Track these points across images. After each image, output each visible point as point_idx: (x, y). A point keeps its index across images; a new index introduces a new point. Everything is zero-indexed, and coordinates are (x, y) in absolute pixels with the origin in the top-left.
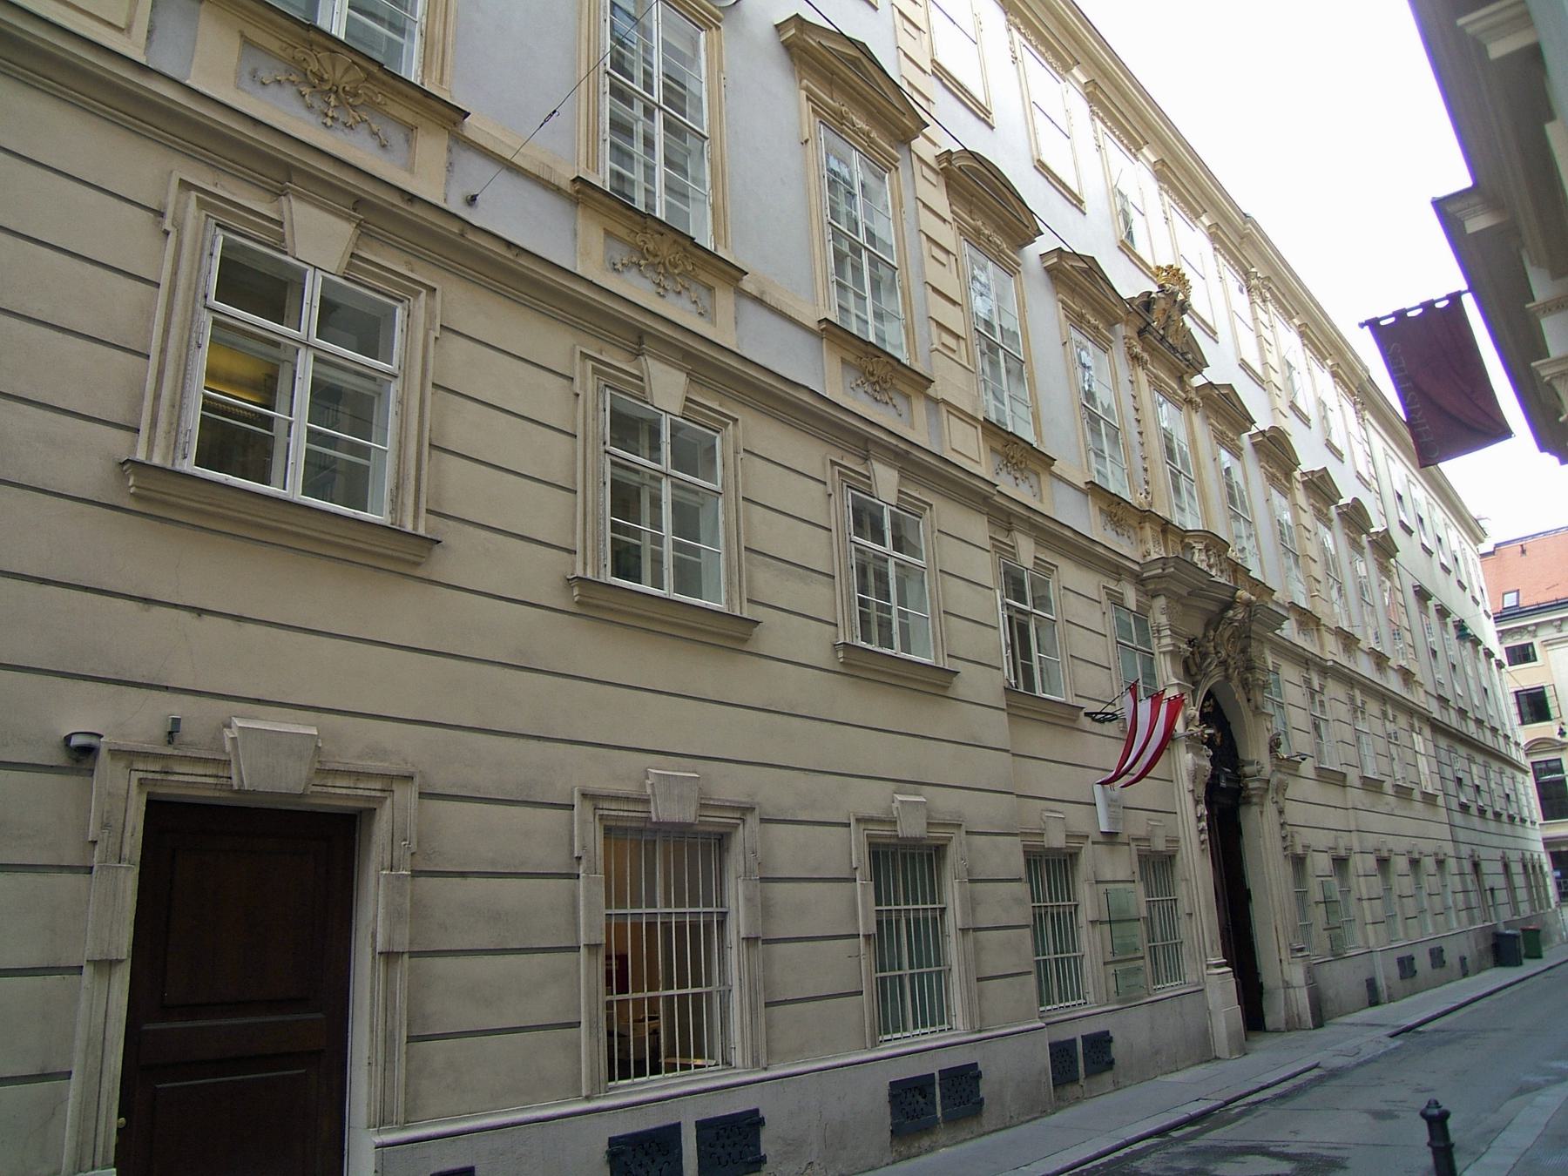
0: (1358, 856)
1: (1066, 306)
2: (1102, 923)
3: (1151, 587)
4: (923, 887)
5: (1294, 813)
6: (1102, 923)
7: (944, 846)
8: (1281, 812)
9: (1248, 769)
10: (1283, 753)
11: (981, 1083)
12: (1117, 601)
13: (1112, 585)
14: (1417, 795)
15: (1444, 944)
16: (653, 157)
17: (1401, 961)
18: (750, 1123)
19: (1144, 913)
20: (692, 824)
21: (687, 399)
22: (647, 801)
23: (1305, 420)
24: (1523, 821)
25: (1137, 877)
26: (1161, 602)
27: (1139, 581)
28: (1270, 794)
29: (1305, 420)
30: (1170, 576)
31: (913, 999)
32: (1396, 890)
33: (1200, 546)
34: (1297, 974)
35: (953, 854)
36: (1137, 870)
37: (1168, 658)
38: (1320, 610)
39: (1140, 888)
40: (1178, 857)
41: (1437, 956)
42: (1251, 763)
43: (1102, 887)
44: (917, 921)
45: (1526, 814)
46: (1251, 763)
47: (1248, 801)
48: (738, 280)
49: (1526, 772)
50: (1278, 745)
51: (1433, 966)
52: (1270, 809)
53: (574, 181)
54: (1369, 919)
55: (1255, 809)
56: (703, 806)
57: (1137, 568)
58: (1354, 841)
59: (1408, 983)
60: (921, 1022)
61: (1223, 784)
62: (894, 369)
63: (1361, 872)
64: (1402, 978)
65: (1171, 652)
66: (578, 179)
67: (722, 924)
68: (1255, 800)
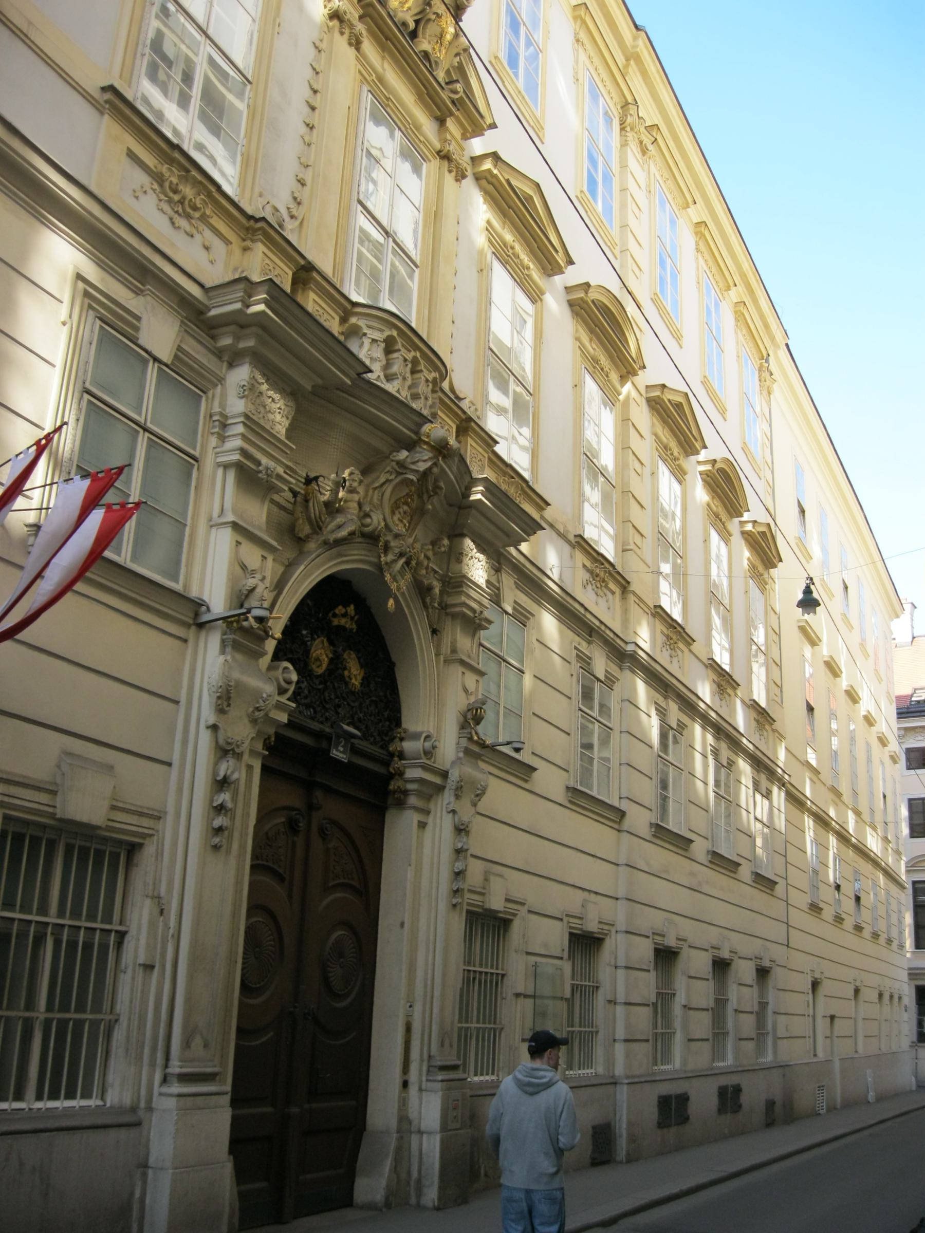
0: (621, 938)
1: (582, 348)
2: (526, 996)
3: (226, 341)
4: (487, 951)
5: (488, 840)
6: (526, 996)
7: (510, 921)
8: (461, 830)
9: (408, 746)
10: (485, 731)
11: (689, 1103)
12: (585, 661)
13: (584, 647)
14: (745, 872)
15: (745, 1082)
16: (190, 87)
17: (664, 1102)
18: (738, 1090)
19: (568, 994)
20: (99, 828)
21: (179, 348)
22: (54, 793)
23: (867, 656)
24: (889, 941)
25: (566, 955)
26: (242, 374)
27: (194, 314)
28: (448, 796)
29: (867, 656)
30: (259, 320)
31: (477, 1055)
32: (680, 999)
33: (376, 335)
34: (429, 1109)
35: (608, 945)
36: (567, 949)
37: (231, 476)
38: (634, 571)
39: (567, 967)
40: (150, 849)
41: (730, 1098)
42: (416, 736)
43: (533, 959)
44: (73, 945)
45: (894, 933)
46: (416, 736)
47: (401, 804)
48: (543, 509)
49: (902, 887)
50: (478, 720)
51: (721, 1110)
52: (441, 826)
53: (104, 89)
54: (620, 1034)
55: (410, 818)
56: (114, 808)
57: (195, 290)
58: (687, 929)
59: (672, 1133)
60: (83, 1097)
61: (339, 753)
62: (728, 682)
63: (621, 962)
64: (661, 1125)
65: (239, 466)
66: (111, 89)
67: (119, 944)
68: (413, 800)
